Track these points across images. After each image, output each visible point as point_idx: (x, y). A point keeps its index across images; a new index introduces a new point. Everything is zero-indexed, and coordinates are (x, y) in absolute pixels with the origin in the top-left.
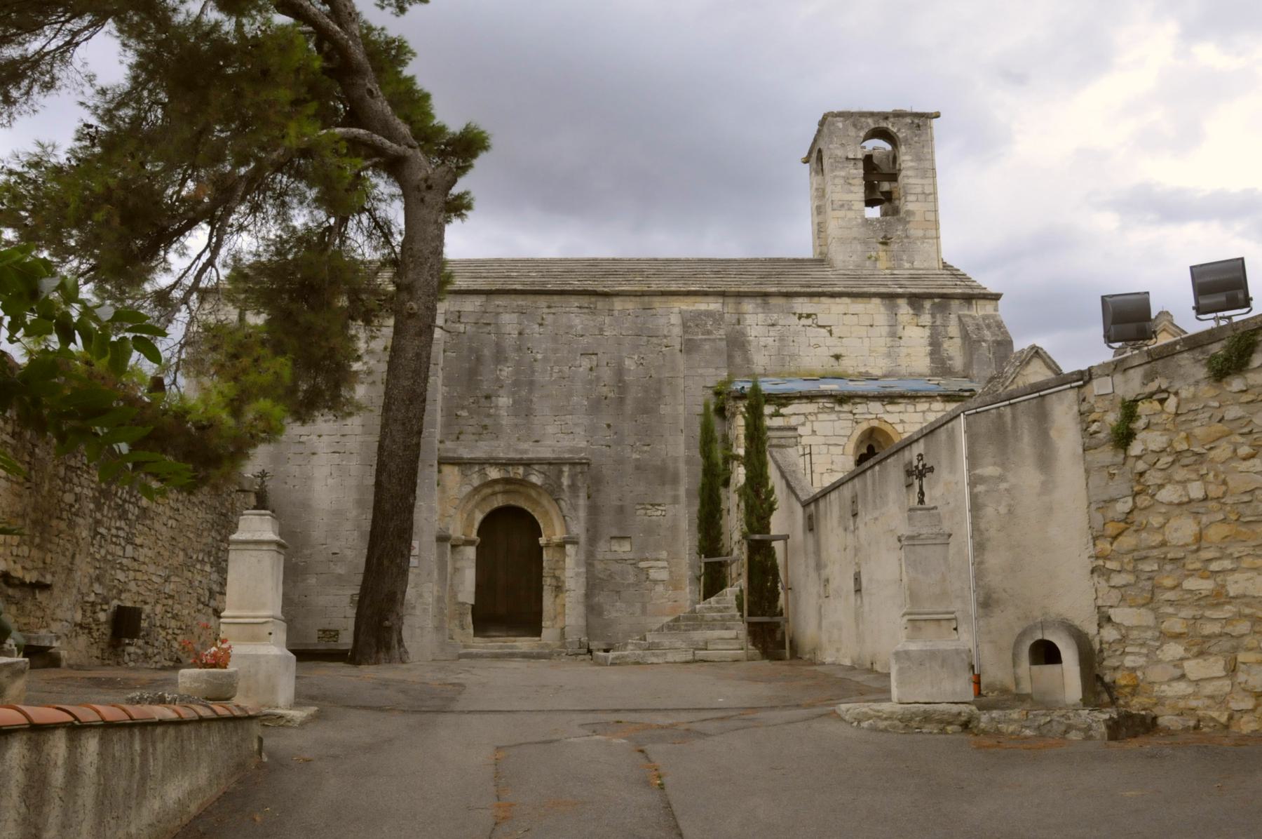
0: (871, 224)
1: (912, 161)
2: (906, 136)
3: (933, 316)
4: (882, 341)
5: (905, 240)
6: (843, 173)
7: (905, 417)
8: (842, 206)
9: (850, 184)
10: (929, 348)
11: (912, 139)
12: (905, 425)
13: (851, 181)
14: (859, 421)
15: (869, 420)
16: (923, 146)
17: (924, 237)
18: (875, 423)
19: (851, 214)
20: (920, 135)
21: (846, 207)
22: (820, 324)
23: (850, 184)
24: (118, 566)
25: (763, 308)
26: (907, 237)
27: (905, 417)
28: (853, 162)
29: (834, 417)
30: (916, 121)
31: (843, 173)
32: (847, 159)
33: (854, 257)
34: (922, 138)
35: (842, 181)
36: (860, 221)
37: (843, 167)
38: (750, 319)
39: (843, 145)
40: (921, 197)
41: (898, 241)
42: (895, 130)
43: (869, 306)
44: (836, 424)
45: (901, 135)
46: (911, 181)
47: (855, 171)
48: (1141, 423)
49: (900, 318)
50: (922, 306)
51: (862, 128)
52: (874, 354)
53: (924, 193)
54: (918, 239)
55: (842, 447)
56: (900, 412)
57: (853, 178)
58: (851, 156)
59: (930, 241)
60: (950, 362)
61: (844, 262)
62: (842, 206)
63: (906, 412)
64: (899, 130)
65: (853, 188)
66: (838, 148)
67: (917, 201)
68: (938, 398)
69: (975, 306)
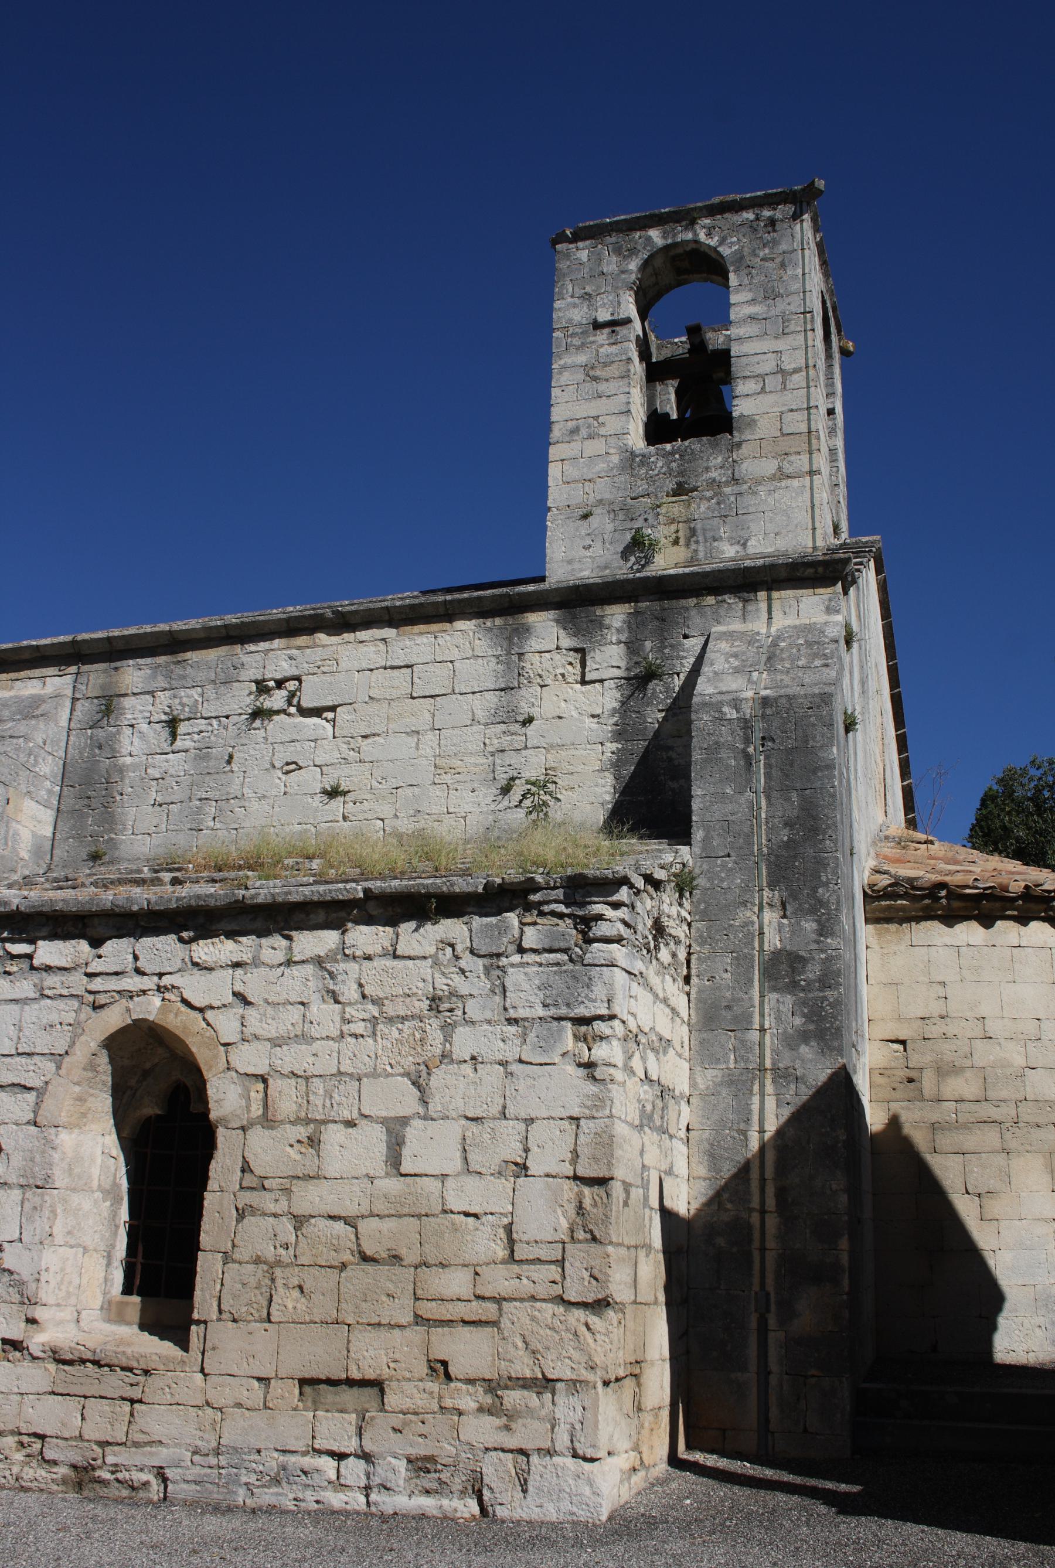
0: (642, 464)
1: (753, 301)
2: (740, 250)
3: (632, 647)
4: (474, 737)
5: (728, 490)
6: (582, 359)
7: (252, 983)
8: (575, 431)
9: (596, 379)
10: (614, 746)
11: (754, 254)
12: (251, 1013)
13: (598, 373)
14: (102, 999)
15: (131, 995)
16: (783, 265)
17: (782, 475)
18: (151, 1008)
19: (597, 447)
20: (775, 242)
21: (584, 432)
22: (306, 703)
23: (596, 379)
24: (489, 1130)
25: (169, 677)
26: (735, 480)
27: (252, 983)
28: (606, 331)
29: (25, 987)
30: (767, 213)
31: (582, 359)
32: (597, 326)
33: (597, 550)
34: (784, 246)
35: (580, 376)
36: (615, 459)
37: (583, 345)
38: (134, 708)
39: (587, 297)
40: (772, 383)
41: (709, 494)
42: (713, 242)
43: (445, 639)
44: (31, 1012)
45: (725, 251)
46: (748, 348)
47: (613, 349)
48: (400, 1026)
49: (534, 663)
50: (600, 624)
51: (633, 252)
52: (447, 778)
53: (782, 371)
54: (759, 481)
55: (31, 1097)
56: (237, 965)
57: (606, 365)
58: (604, 316)
59: (795, 483)
60: (674, 785)
61: (570, 562)
62: (575, 431)
63: (257, 962)
64: (723, 241)
65: (603, 387)
66: (575, 306)
67: (763, 390)
68: (373, 909)
69: (763, 606)
